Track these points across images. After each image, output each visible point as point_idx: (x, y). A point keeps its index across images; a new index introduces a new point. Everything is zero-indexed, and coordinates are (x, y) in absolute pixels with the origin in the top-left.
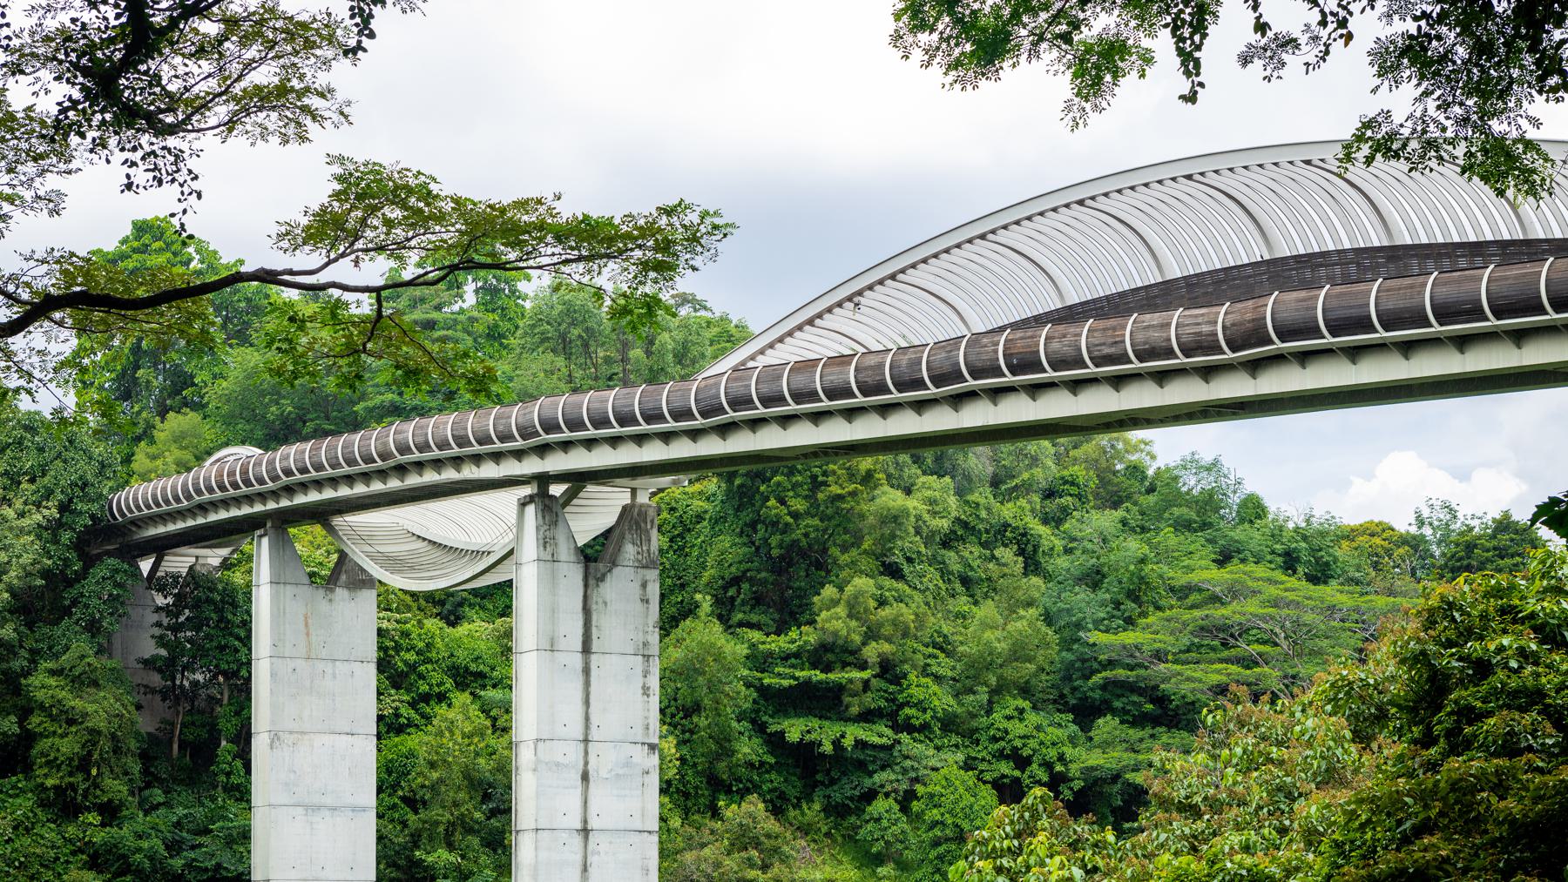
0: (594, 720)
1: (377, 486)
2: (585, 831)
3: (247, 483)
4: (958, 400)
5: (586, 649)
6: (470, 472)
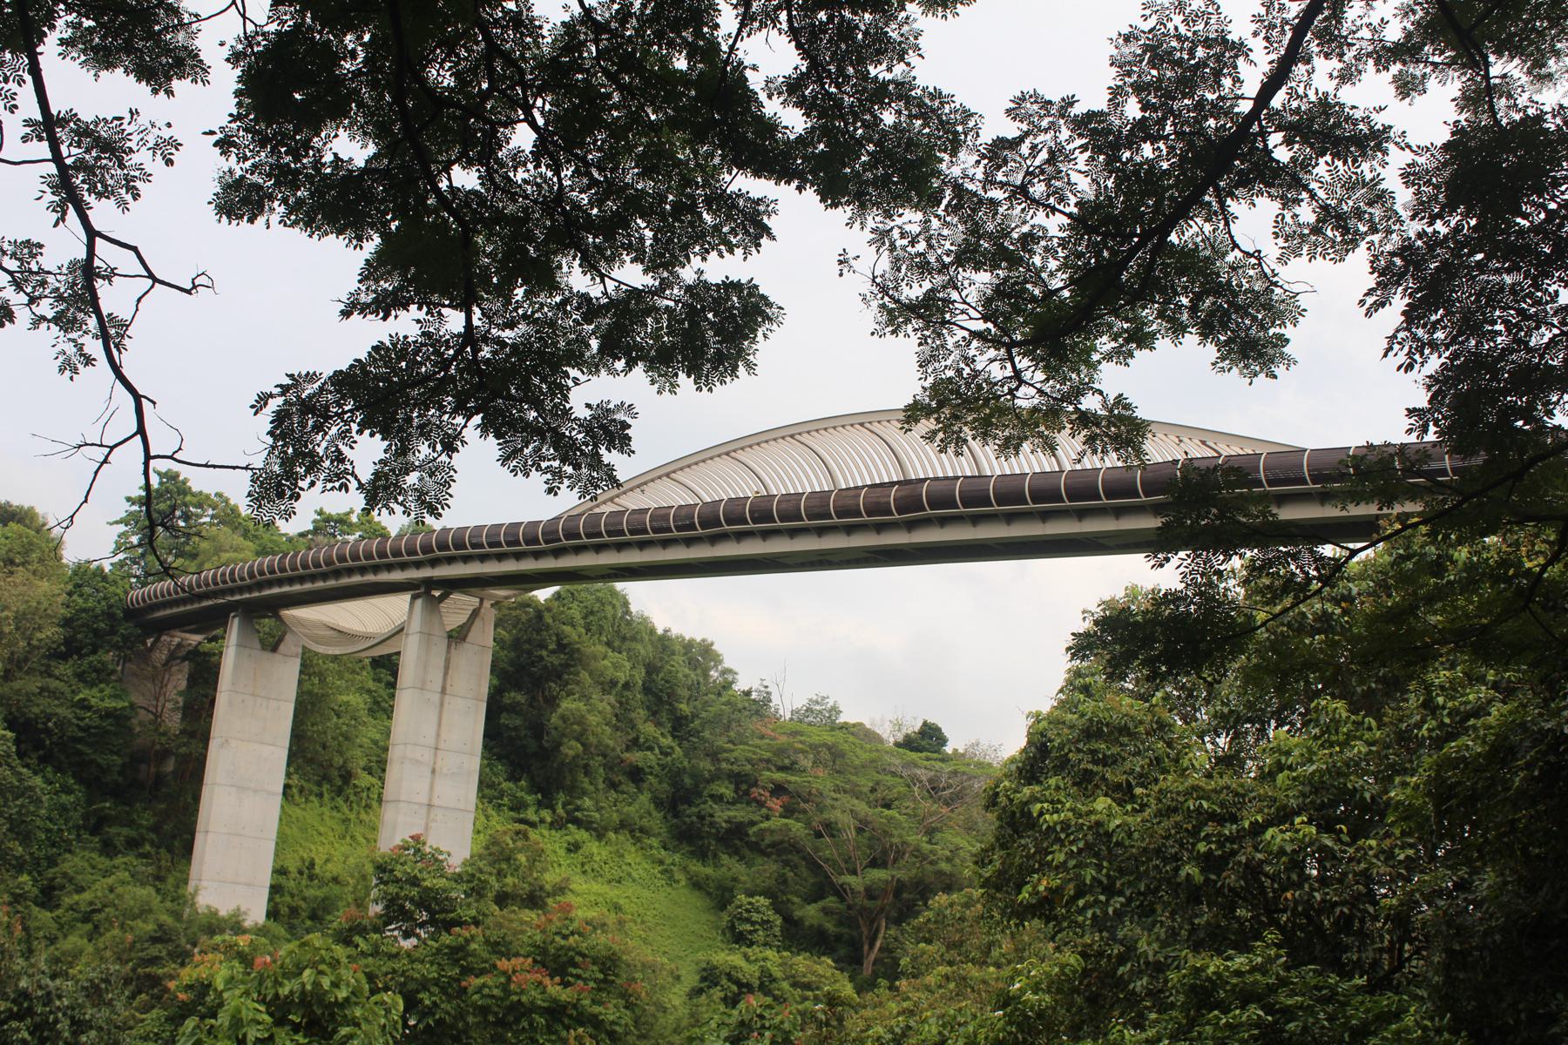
0: (444, 735)
1: (320, 584)
2: (430, 806)
3: (233, 580)
4: (714, 539)
5: (443, 691)
6: (384, 577)
